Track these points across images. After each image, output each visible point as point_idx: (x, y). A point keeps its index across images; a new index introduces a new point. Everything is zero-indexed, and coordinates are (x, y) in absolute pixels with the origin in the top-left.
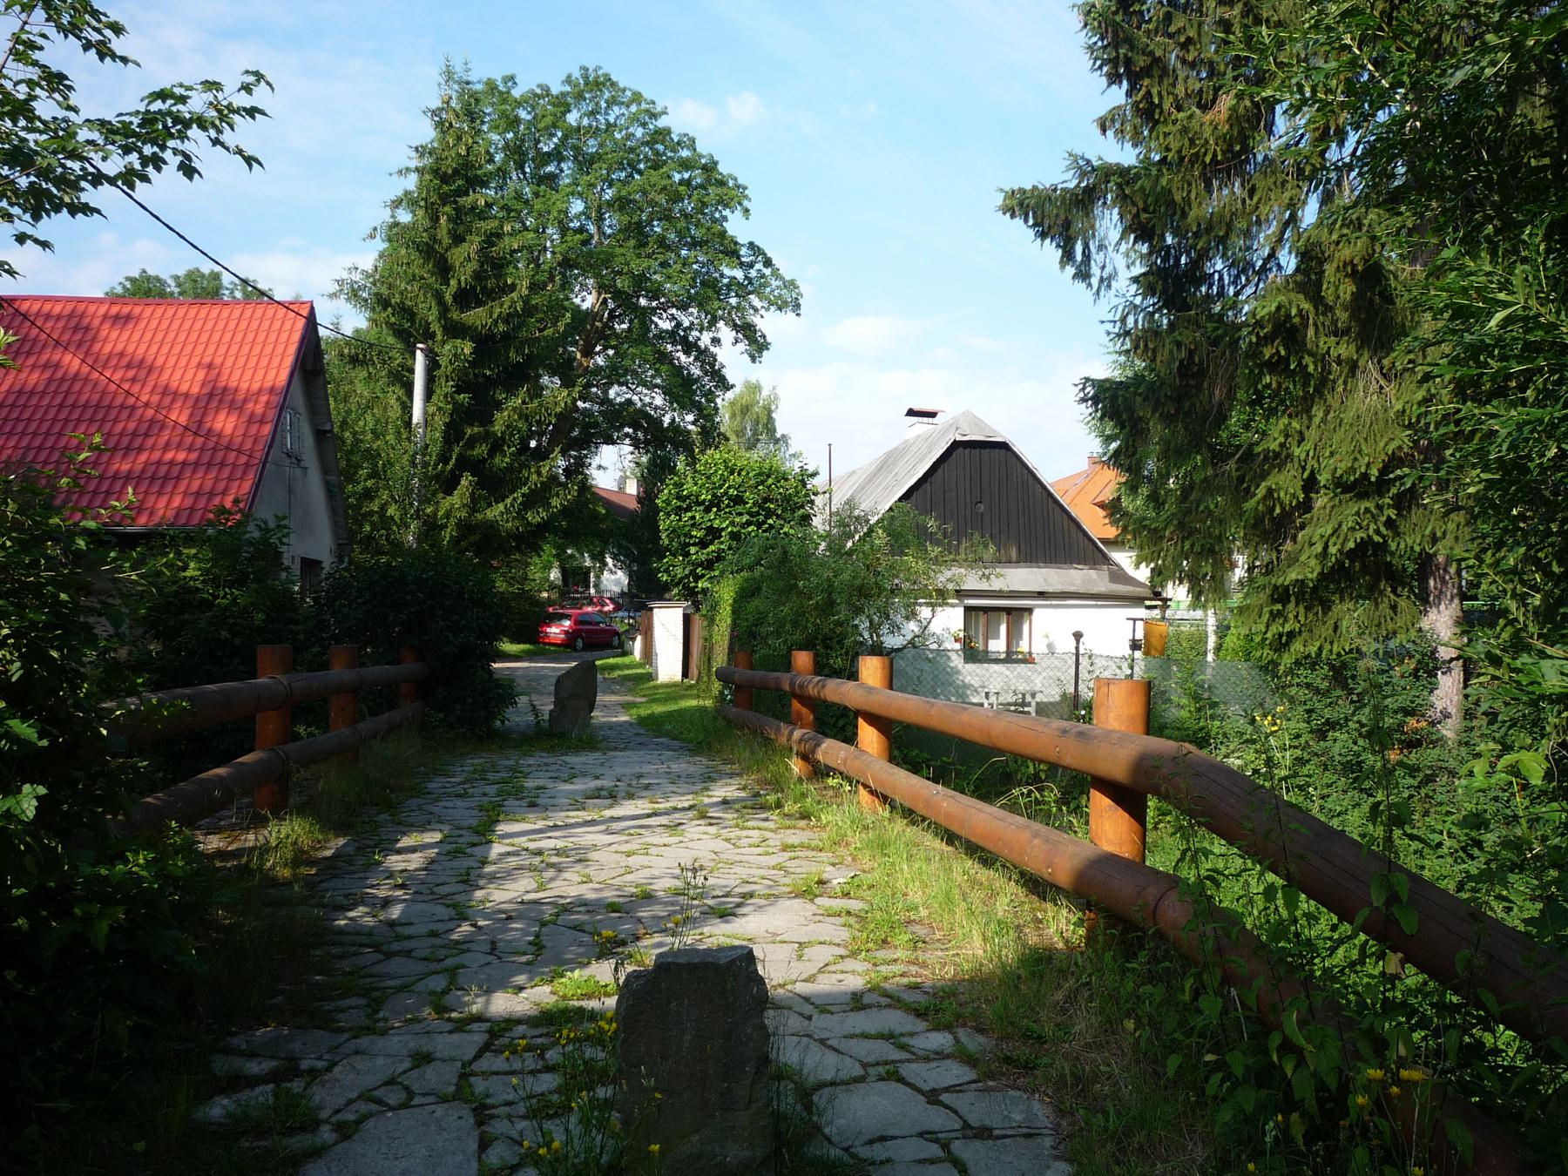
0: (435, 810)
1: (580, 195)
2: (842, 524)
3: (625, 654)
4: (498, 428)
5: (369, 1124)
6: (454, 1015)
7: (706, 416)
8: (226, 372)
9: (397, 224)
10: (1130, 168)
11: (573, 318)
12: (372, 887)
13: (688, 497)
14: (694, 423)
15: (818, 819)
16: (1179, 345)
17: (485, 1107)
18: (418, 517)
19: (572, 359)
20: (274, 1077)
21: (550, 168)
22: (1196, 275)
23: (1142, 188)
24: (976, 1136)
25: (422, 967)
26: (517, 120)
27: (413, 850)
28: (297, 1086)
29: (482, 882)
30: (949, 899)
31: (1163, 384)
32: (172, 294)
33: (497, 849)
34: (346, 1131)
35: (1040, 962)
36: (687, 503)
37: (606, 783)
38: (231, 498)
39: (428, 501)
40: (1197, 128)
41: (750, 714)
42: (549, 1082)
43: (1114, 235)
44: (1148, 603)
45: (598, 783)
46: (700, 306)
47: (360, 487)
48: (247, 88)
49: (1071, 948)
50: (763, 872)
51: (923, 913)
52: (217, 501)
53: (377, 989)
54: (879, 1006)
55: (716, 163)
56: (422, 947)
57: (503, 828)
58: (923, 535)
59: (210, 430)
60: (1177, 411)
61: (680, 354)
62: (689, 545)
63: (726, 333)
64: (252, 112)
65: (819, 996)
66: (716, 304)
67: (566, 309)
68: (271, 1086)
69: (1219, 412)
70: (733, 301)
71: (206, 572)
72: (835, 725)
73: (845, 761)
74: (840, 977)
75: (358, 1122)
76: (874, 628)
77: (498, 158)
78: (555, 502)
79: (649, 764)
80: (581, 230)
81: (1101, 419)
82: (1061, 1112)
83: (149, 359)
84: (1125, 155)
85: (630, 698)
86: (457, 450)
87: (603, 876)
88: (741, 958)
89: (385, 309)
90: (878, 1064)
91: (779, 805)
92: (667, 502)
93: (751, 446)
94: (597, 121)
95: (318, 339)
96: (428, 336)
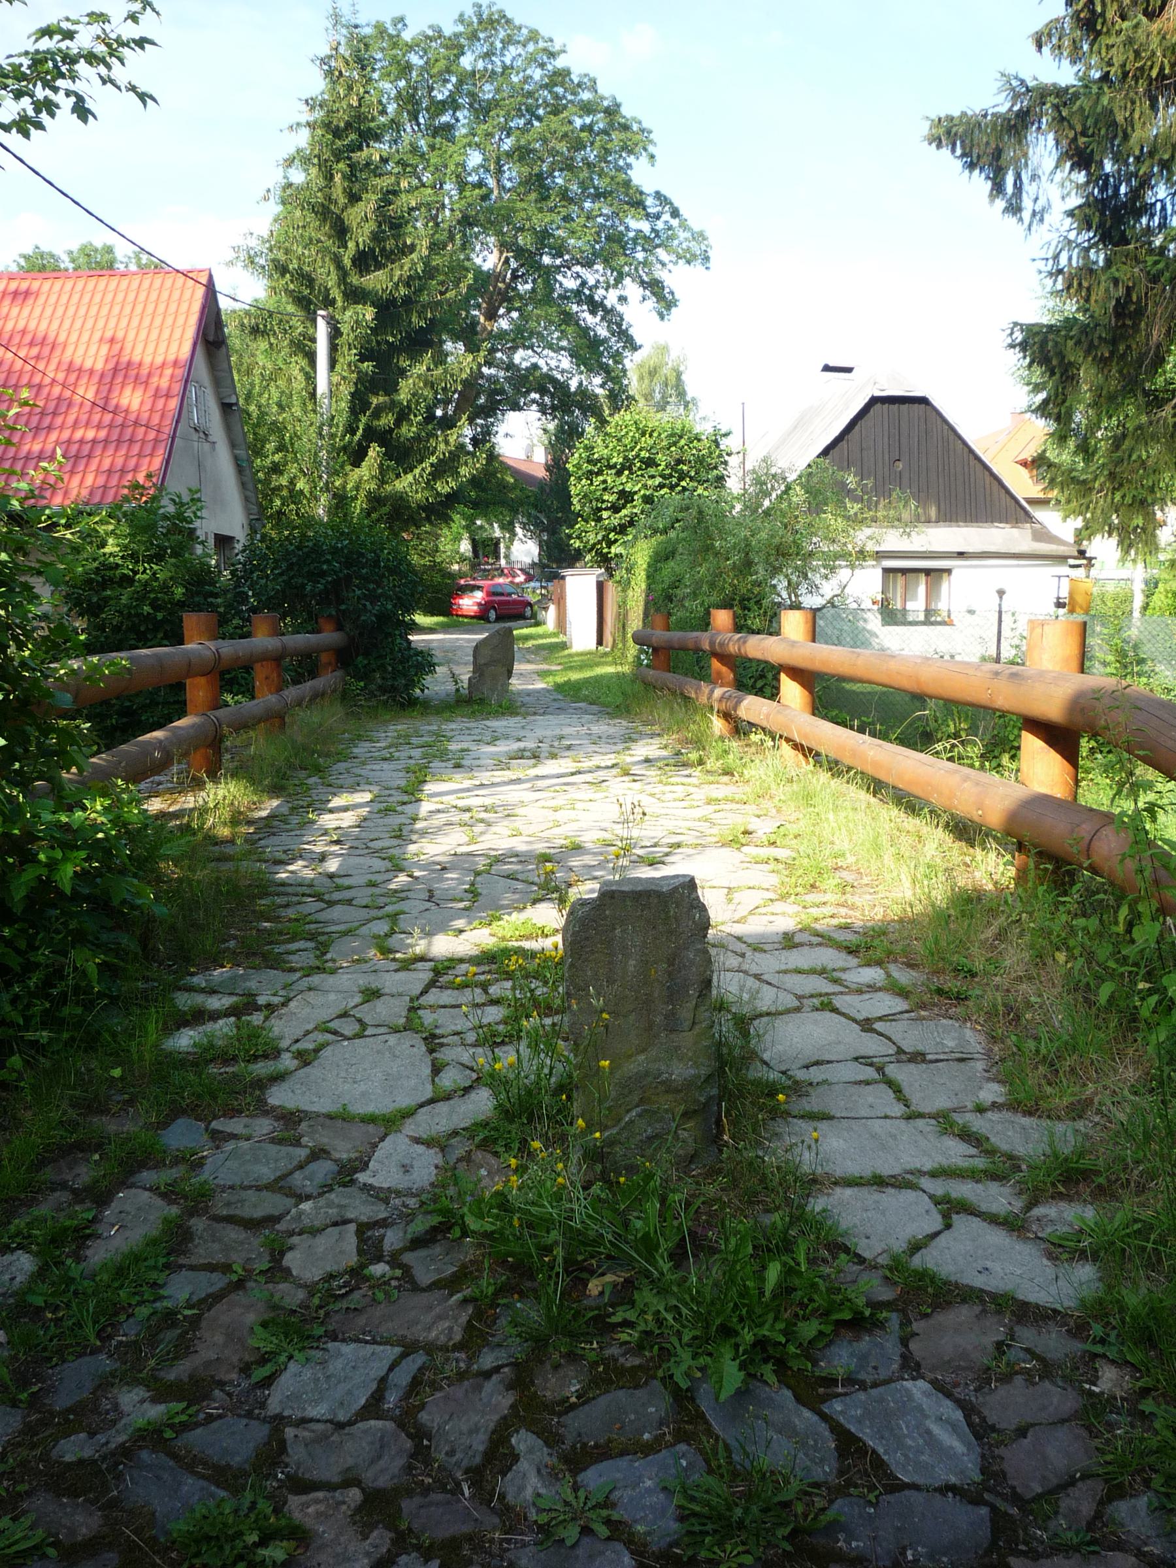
0: (363, 772)
1: (478, 145)
2: (758, 482)
3: (538, 624)
4: (403, 396)
5: (326, 1053)
6: (398, 955)
7: (614, 377)
8: (128, 346)
9: (290, 185)
10: (1067, 88)
11: (475, 279)
12: (308, 843)
13: (599, 461)
14: (602, 386)
15: (741, 775)
16: (1116, 281)
17: (434, 1036)
18: (328, 490)
19: (474, 323)
20: (234, 1012)
21: (446, 118)
22: (1136, 206)
23: (1081, 109)
24: (909, 1061)
25: (364, 914)
26: (409, 67)
27: (345, 809)
28: (257, 1019)
29: (414, 837)
30: (877, 846)
31: (1097, 325)
32: (66, 270)
33: (425, 807)
34: (305, 1059)
35: (970, 903)
36: (596, 467)
37: (530, 744)
38: (144, 474)
39: (336, 473)
40: (1143, 39)
41: (669, 676)
42: (493, 1014)
43: (1049, 162)
44: (1072, 562)
45: (521, 745)
46: (606, 262)
47: (268, 461)
48: (133, 17)
49: (1000, 890)
50: (691, 824)
51: (851, 859)
52: (129, 477)
53: (324, 934)
54: (811, 945)
55: (618, 106)
56: (362, 896)
57: (430, 788)
58: (843, 491)
59: (117, 406)
60: (1112, 353)
61: (586, 315)
62: (600, 510)
63: (631, 288)
64: (141, 43)
65: (750, 936)
66: (622, 260)
67: (467, 270)
68: (232, 1019)
69: (1157, 354)
70: (640, 256)
71: (125, 548)
72: (753, 687)
73: (768, 716)
74: (772, 918)
75: (317, 1051)
76: (792, 587)
77: (391, 108)
78: (464, 471)
79: (570, 727)
80: (480, 184)
81: (1030, 365)
82: (993, 1039)
83: (52, 336)
84: (1062, 73)
85: (545, 667)
86: (364, 419)
87: (532, 829)
88: (683, 885)
89: (283, 275)
90: (812, 996)
91: (701, 762)
92: (578, 466)
93: (662, 407)
94: (493, 63)
95: (218, 311)
96: (329, 303)
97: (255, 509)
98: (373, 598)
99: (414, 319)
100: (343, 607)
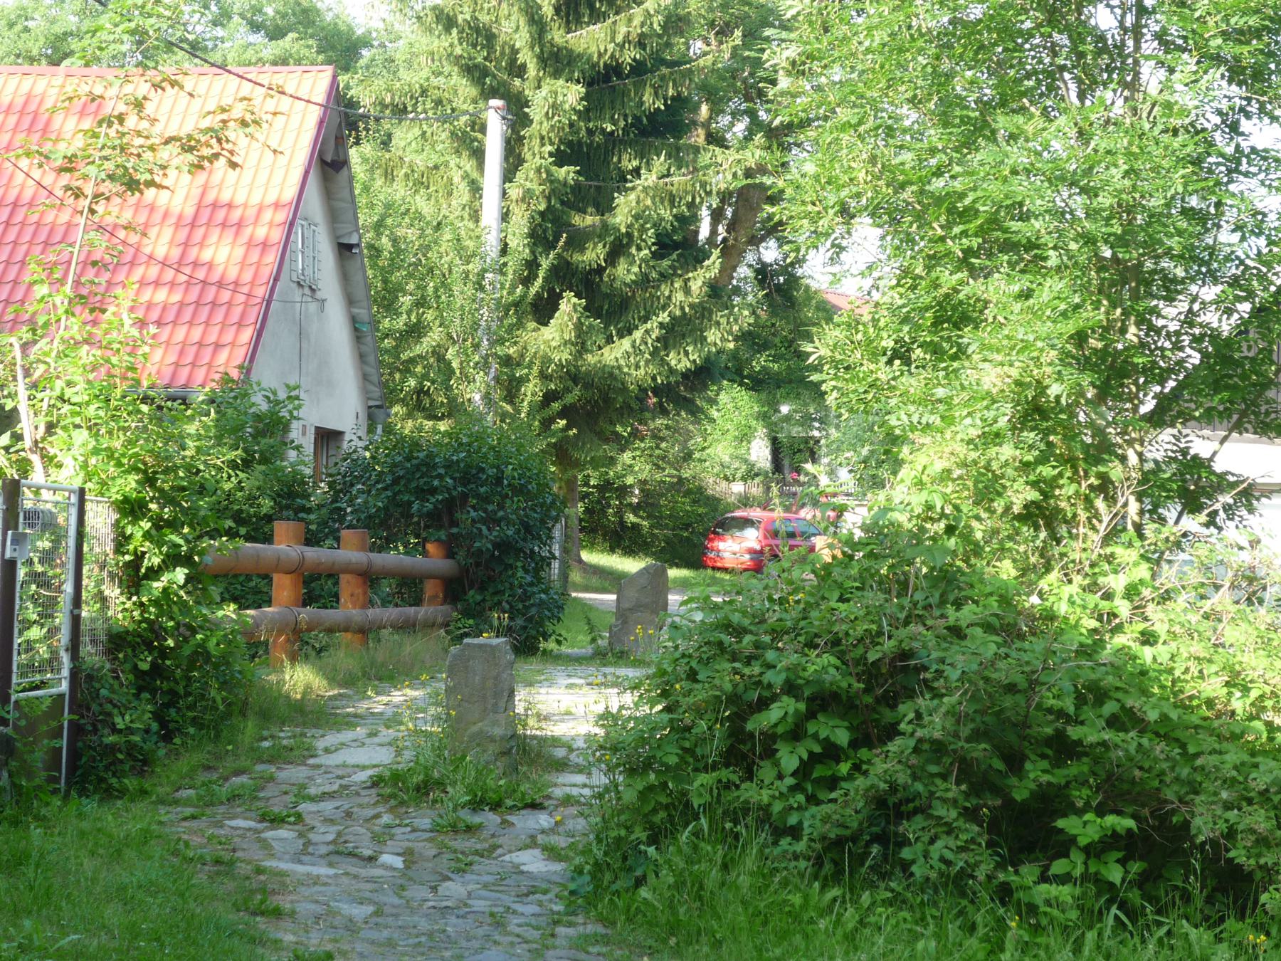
4: (621, 217)
78: (713, 336)
89: (448, 29)
97: (376, 391)
98: (491, 521)
99: (648, 98)
100: (455, 530)
